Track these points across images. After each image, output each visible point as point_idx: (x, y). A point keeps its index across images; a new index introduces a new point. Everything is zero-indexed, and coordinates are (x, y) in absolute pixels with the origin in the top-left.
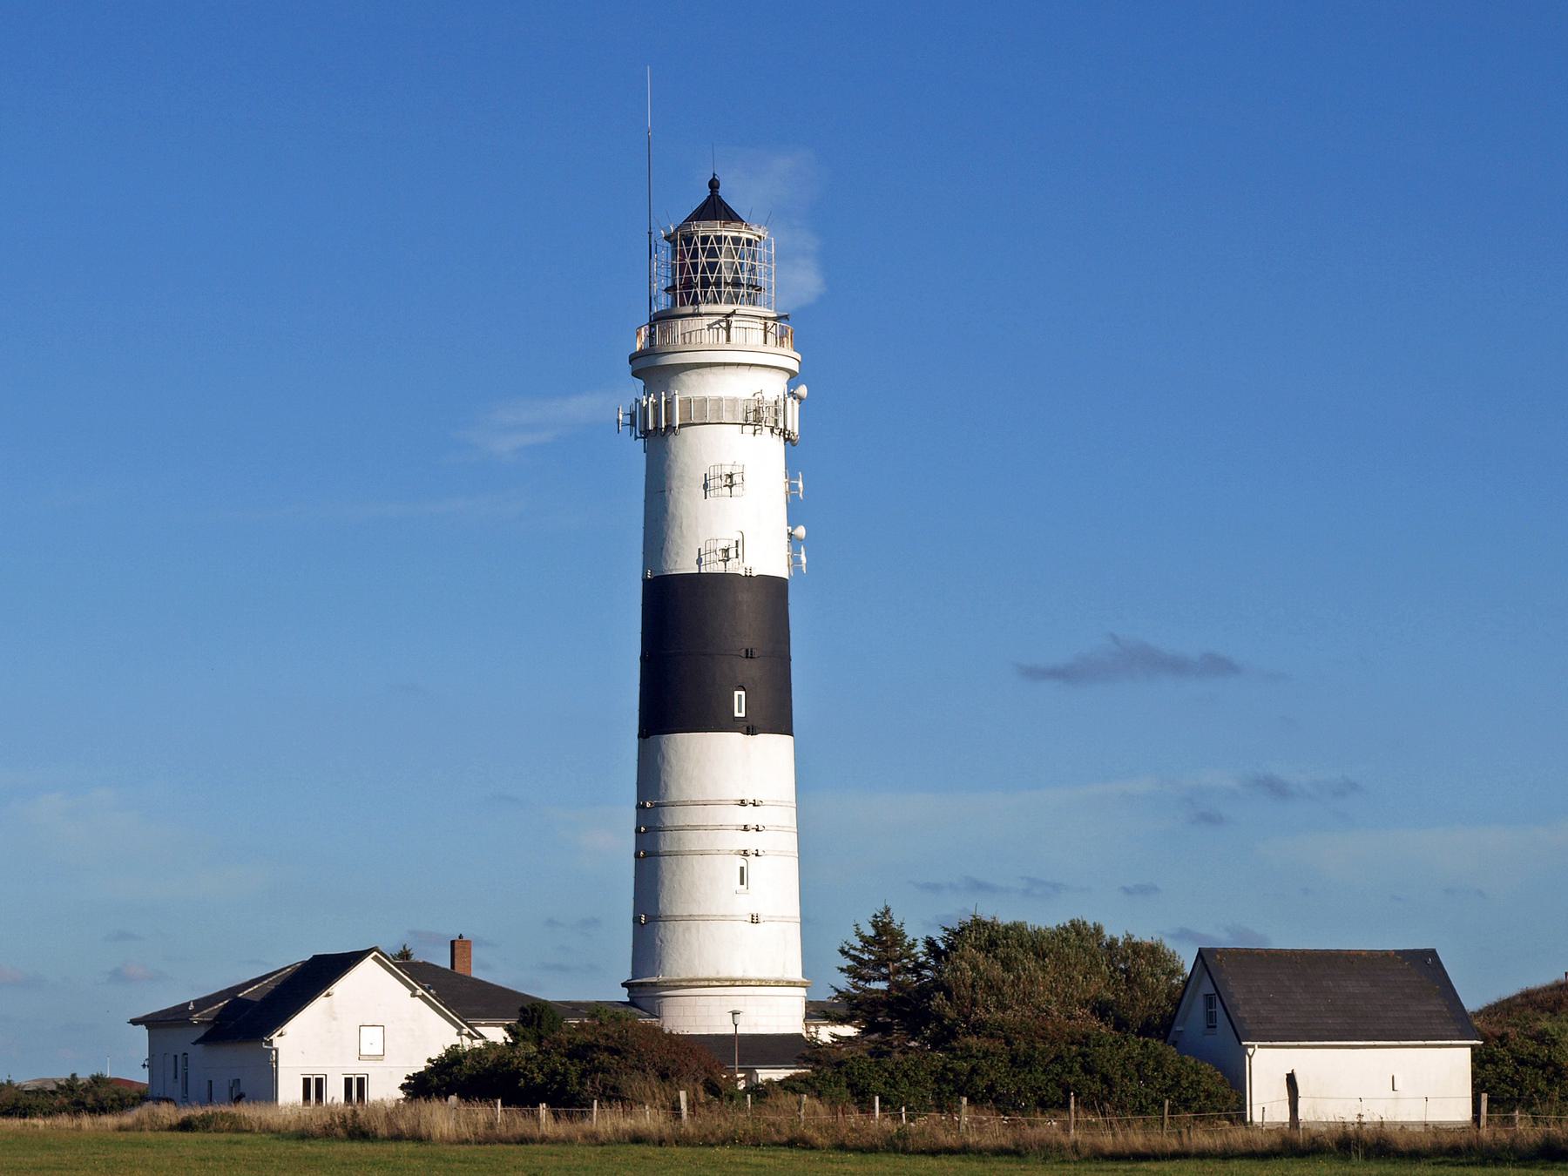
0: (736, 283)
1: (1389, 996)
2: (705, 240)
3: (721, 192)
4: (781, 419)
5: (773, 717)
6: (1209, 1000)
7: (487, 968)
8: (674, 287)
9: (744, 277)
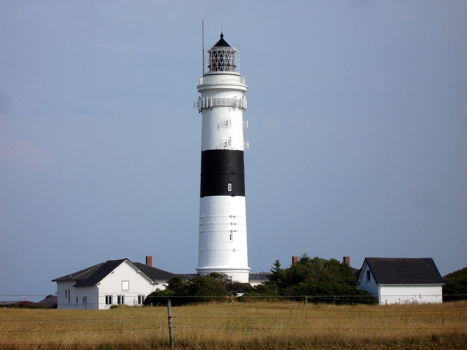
0: (229, 65)
1: (417, 271)
2: (219, 52)
3: (224, 38)
4: (242, 105)
5: (240, 191)
6: (368, 272)
7: (156, 264)
8: (210, 66)
9: (231, 63)
